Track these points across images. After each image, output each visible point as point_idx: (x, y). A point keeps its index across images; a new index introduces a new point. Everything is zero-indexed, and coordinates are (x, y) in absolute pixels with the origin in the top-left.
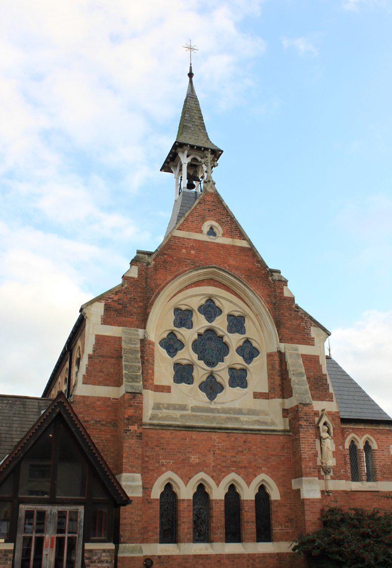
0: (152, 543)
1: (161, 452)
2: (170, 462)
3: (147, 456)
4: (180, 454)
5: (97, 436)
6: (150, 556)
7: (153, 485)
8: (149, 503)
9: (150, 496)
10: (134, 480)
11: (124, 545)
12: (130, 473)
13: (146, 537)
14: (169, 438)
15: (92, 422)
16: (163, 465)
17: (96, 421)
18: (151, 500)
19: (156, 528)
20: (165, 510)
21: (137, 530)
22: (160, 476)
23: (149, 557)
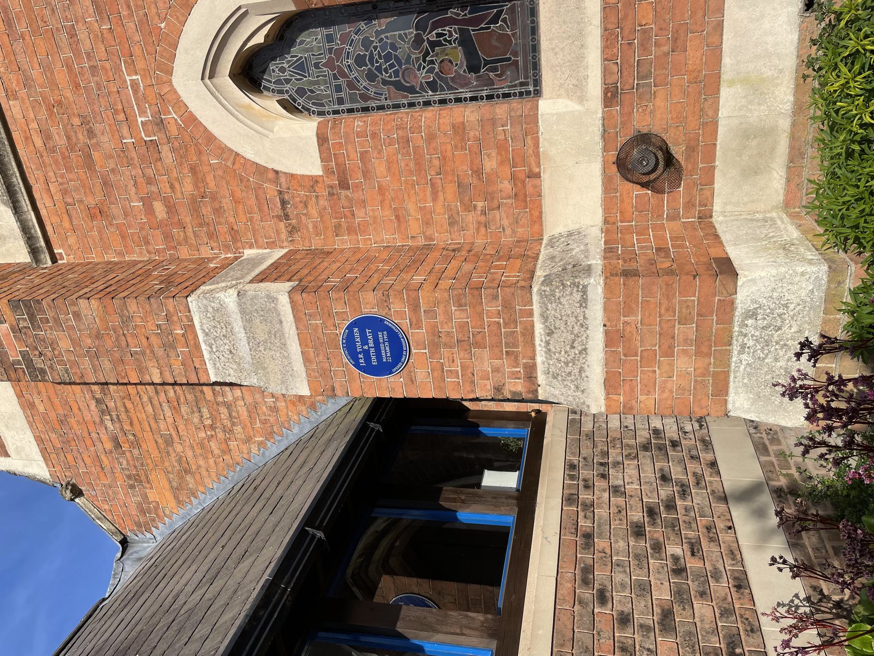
0: (537, 145)
1: (107, 142)
2: (134, 84)
3: (149, 210)
4: (82, 35)
5: (149, 409)
6: (605, 149)
7: (261, 170)
8: (344, 185)
9: (314, 181)
10: (219, 314)
11: (541, 379)
12: (197, 346)
13: (506, 186)
14: (35, 105)
15: (109, 424)
16: (160, 124)
17: (103, 412)
18: (327, 170)
19: (460, 129)
20: (371, 77)
21: (459, 316)
22: (210, 138)
23: (613, 155)
